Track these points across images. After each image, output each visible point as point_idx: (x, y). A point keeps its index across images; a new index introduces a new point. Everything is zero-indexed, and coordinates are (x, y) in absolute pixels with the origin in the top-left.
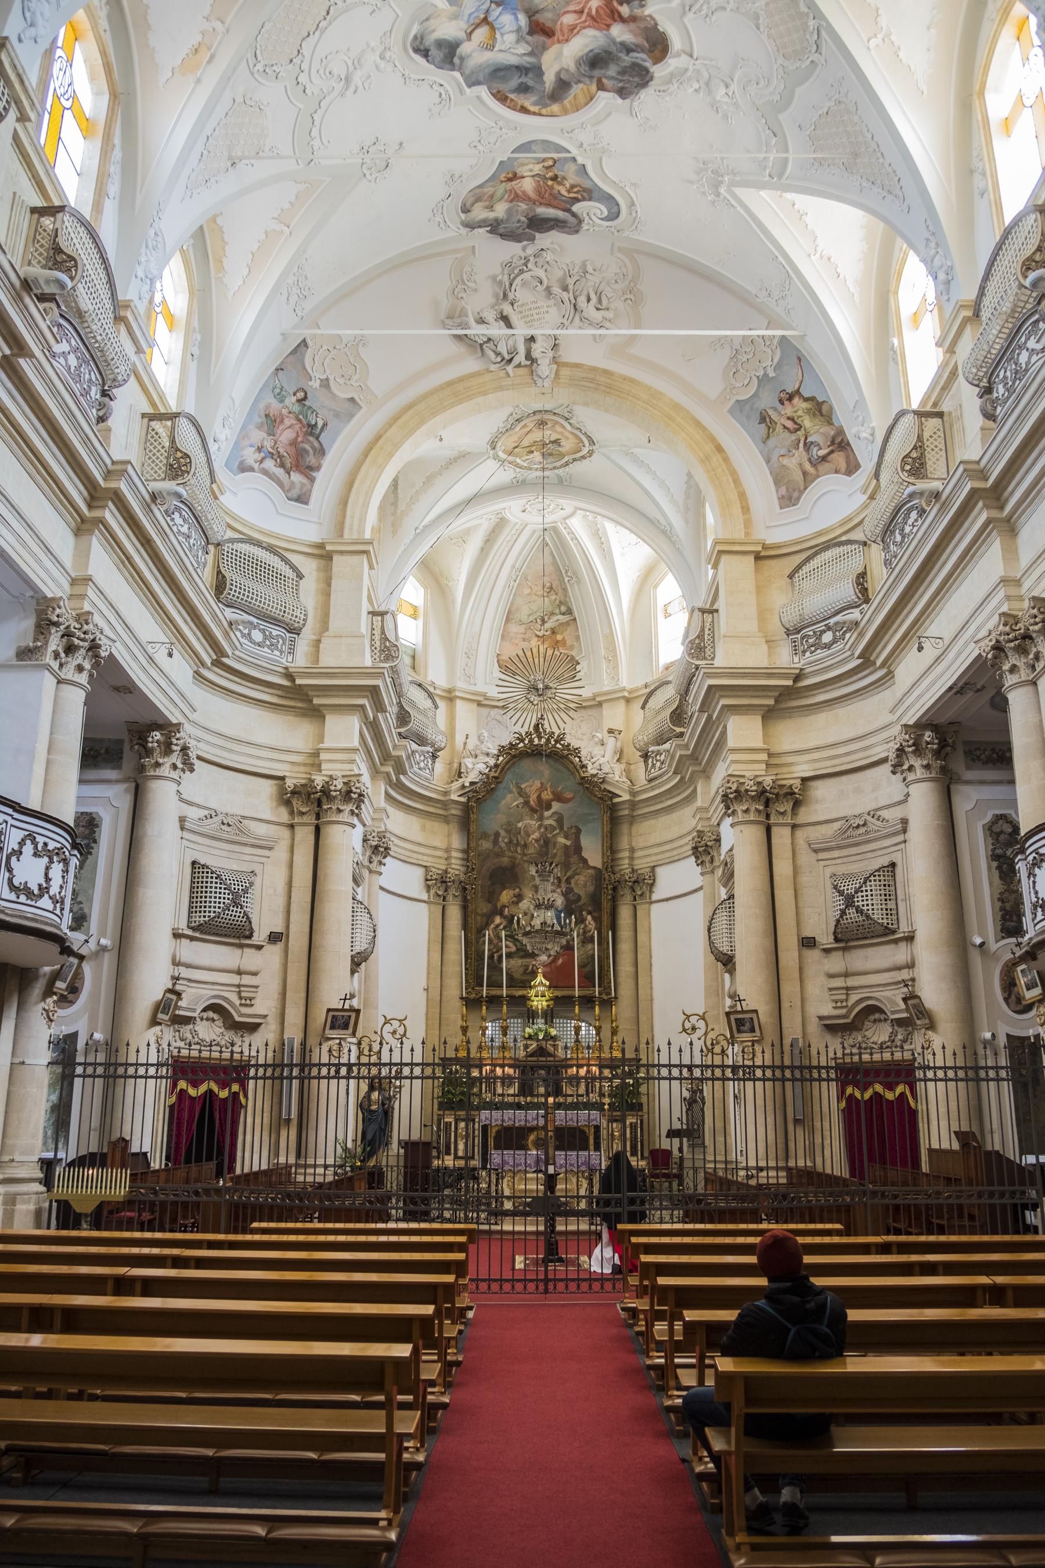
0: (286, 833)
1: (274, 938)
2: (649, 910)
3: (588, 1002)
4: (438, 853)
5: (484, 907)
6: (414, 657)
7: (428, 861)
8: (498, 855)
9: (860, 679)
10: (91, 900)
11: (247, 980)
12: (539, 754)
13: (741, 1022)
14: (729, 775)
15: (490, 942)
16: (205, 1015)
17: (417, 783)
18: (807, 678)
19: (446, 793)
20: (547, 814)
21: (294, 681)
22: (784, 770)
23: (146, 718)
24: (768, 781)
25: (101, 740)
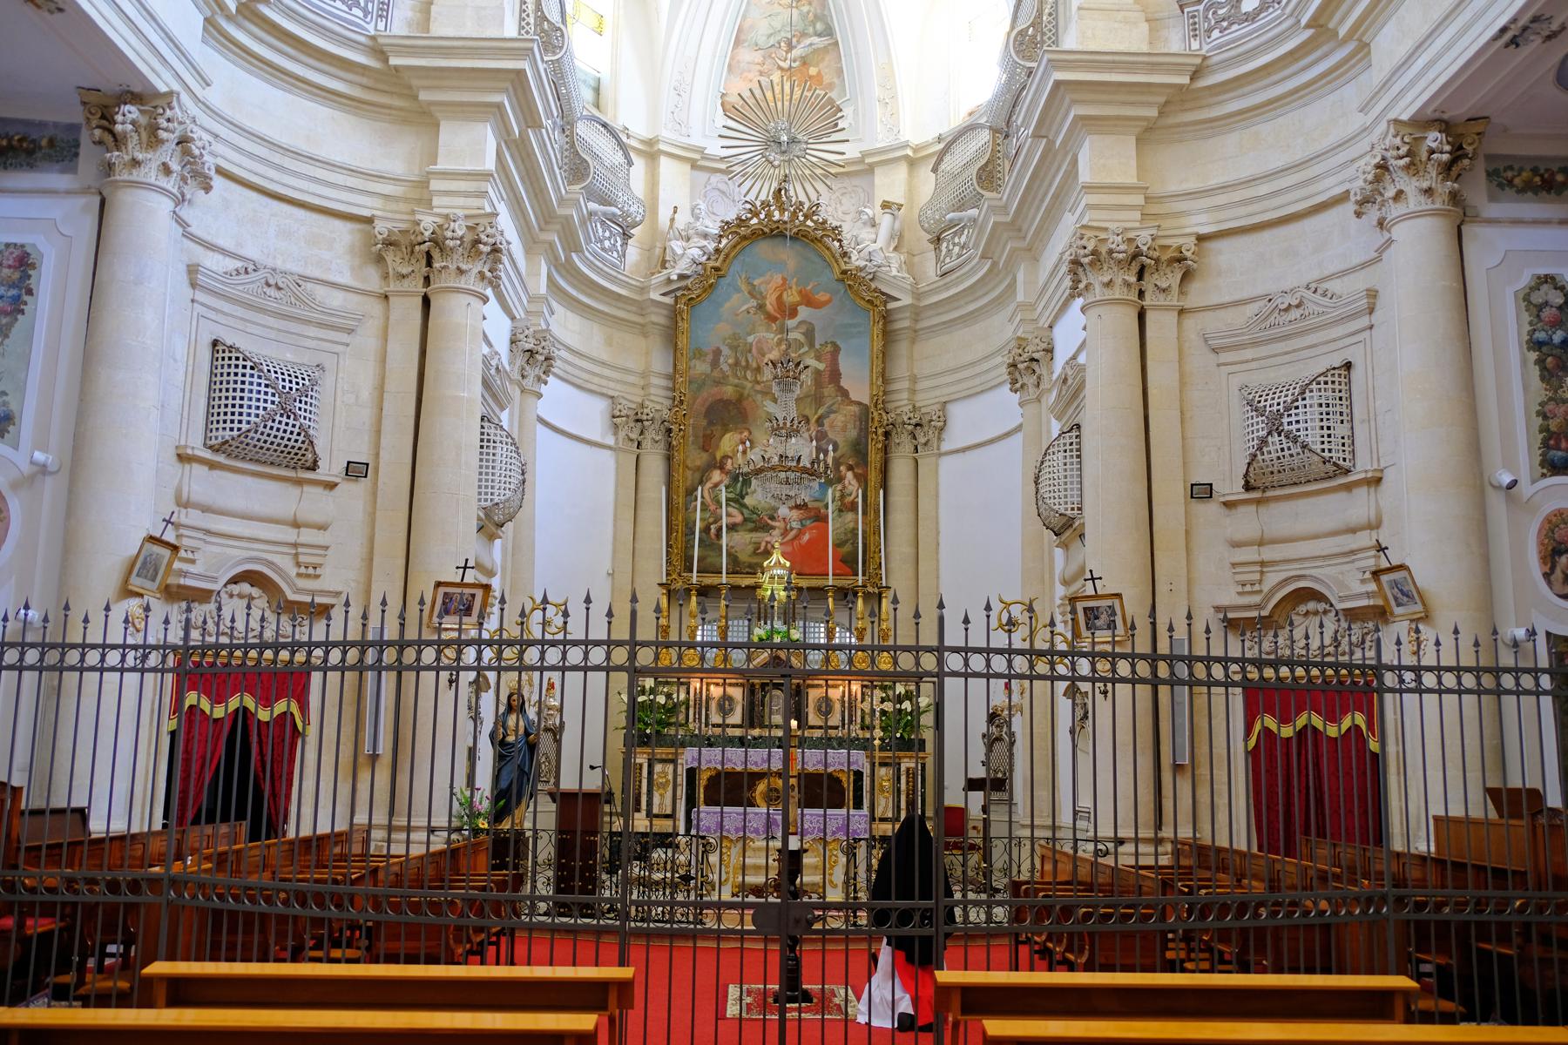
0: (376, 307)
1: (355, 470)
2: (937, 465)
3: (846, 595)
4: (632, 379)
5: (698, 458)
6: (597, 90)
7: (615, 389)
8: (718, 383)
9: (1304, 69)
10: (22, 389)
11: (307, 536)
12: (779, 233)
13: (1091, 612)
14: (1083, 227)
15: (704, 507)
16: (236, 589)
17: (599, 271)
18: (1213, 72)
19: (643, 290)
20: (791, 323)
21: (386, 61)
22: (1166, 224)
23: (111, 83)
24: (1144, 238)
25: (42, 125)
